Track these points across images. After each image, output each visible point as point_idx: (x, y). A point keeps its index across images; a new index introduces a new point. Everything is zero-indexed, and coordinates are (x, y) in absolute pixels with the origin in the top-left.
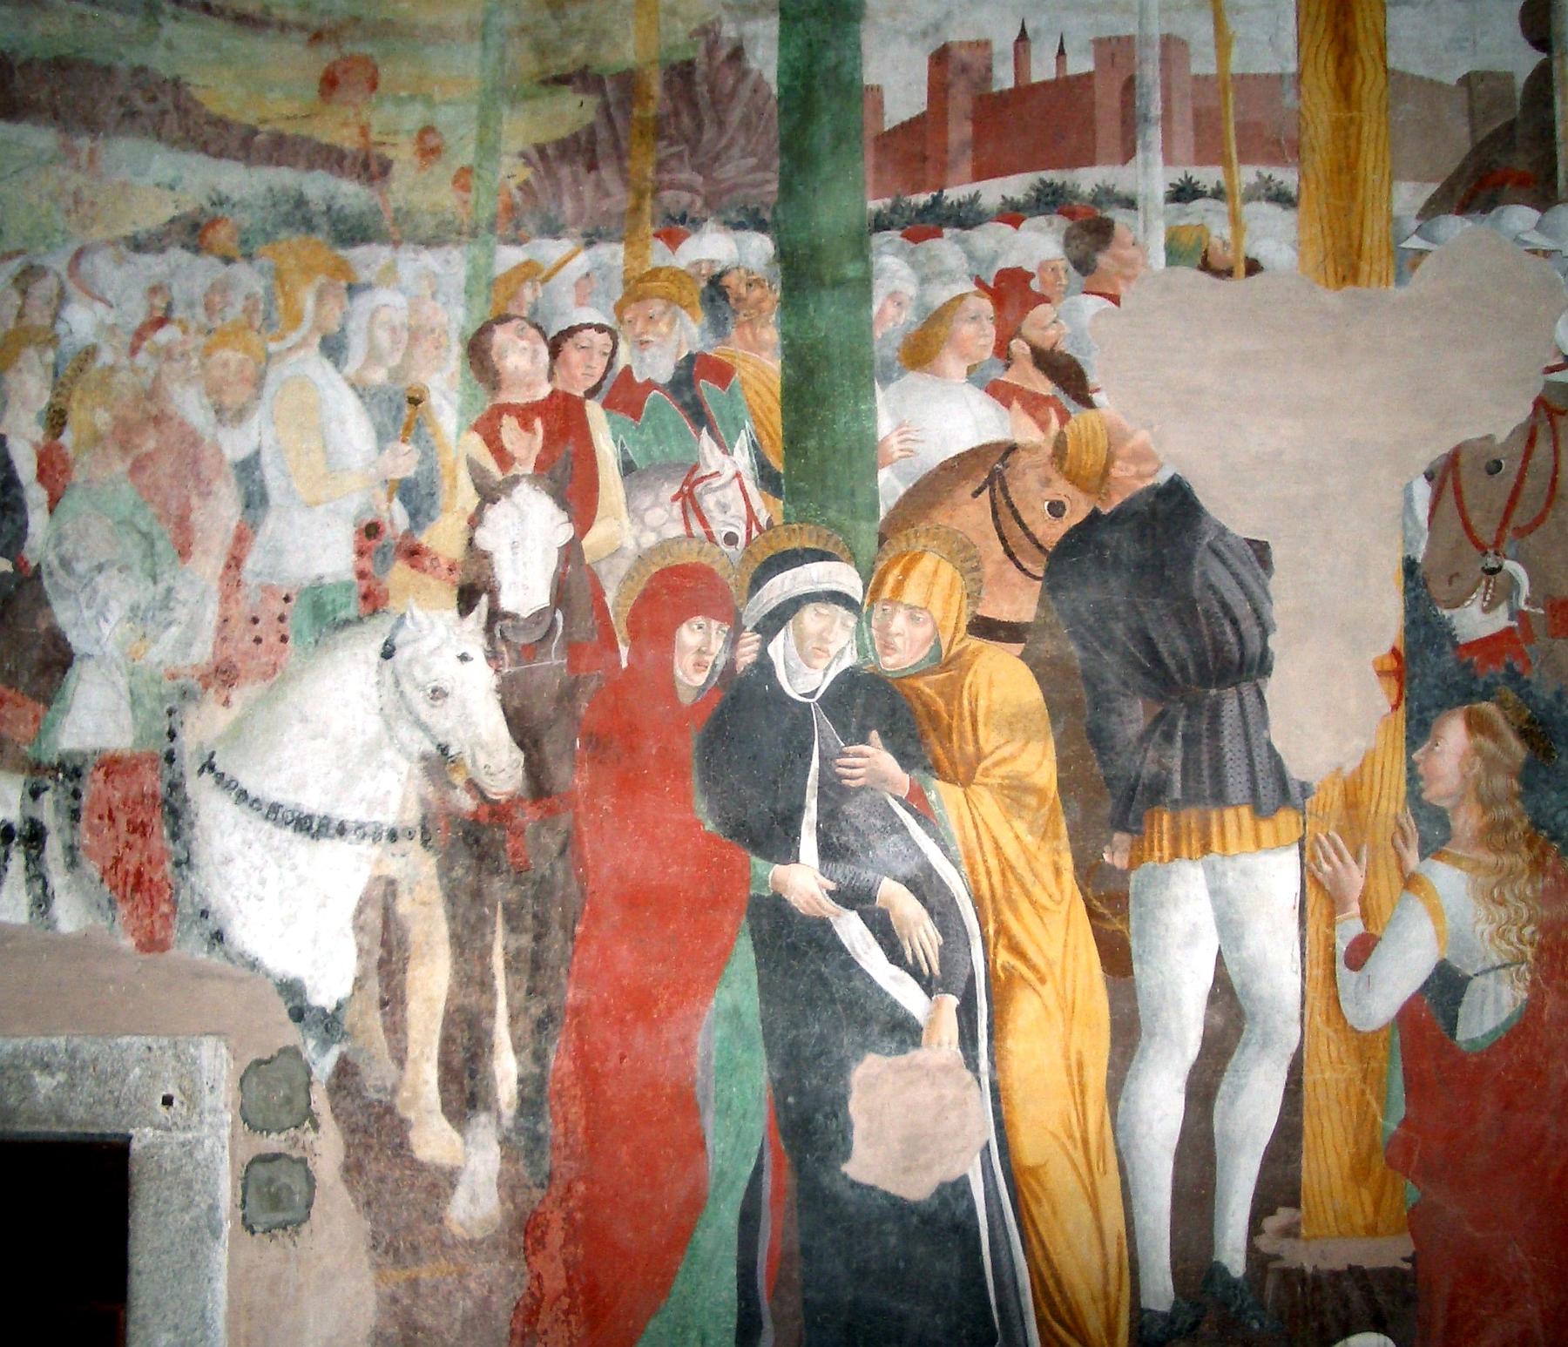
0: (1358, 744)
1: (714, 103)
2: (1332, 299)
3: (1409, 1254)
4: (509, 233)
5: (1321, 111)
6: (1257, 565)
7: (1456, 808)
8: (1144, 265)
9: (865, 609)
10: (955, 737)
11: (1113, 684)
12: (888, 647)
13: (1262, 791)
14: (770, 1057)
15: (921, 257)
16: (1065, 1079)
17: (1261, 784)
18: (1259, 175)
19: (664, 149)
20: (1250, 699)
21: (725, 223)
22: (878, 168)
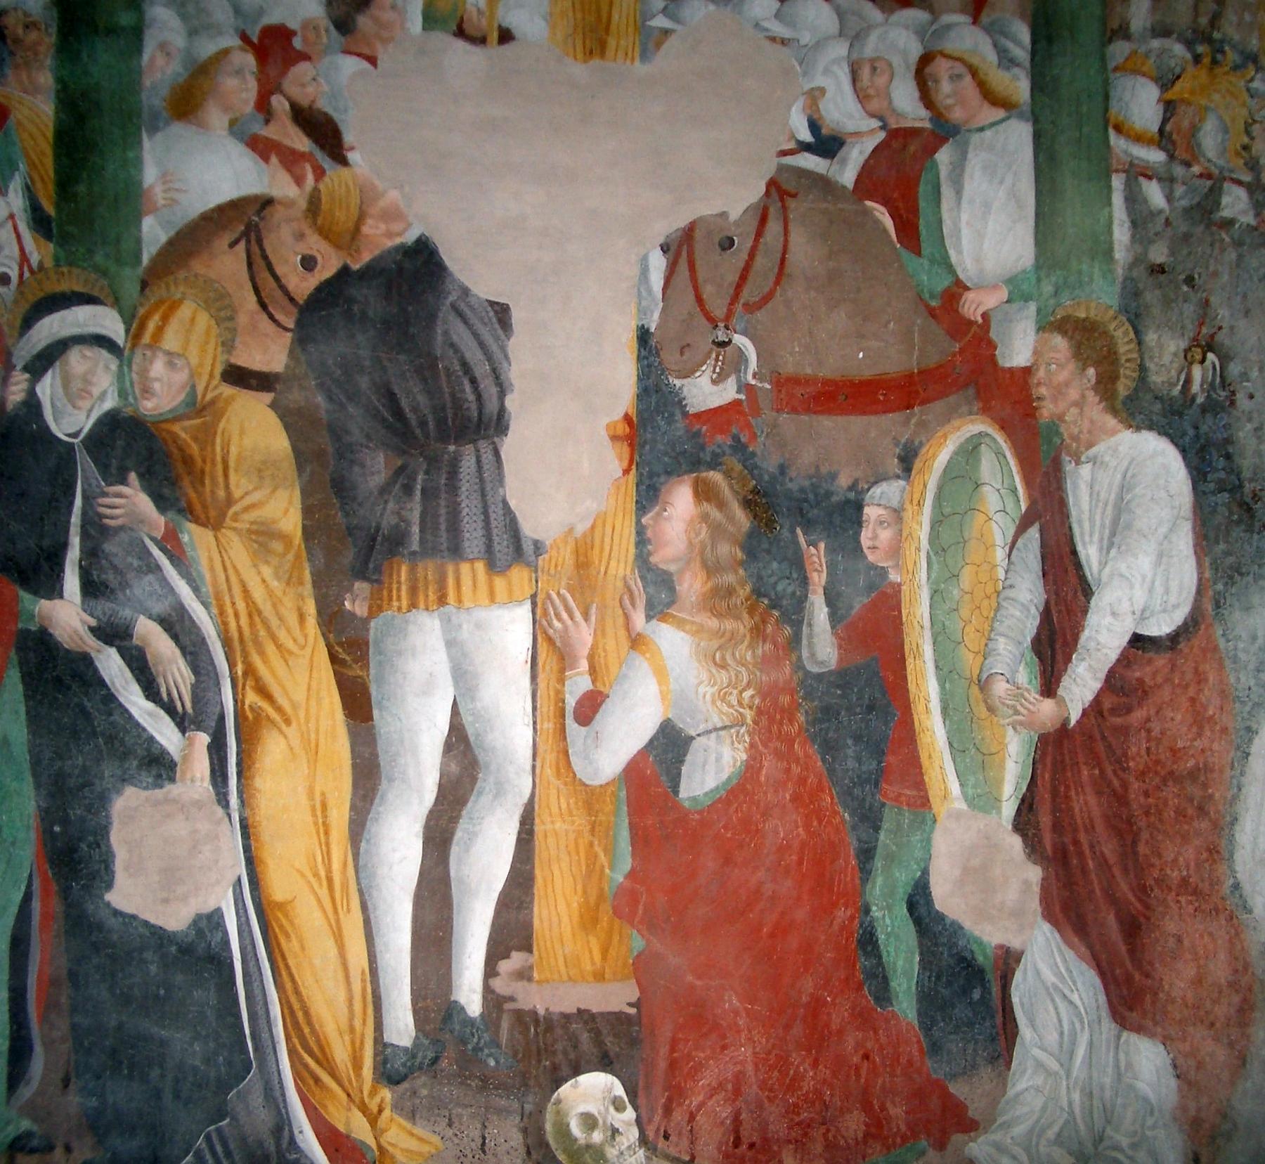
0: (590, 506)
2: (579, 70)
3: (634, 999)
6: (497, 326)
7: (681, 572)
9: (126, 353)
10: (207, 482)
11: (356, 435)
12: (147, 391)
13: (497, 548)
14: (38, 786)
16: (309, 819)
17: (496, 539)
20: (487, 457)
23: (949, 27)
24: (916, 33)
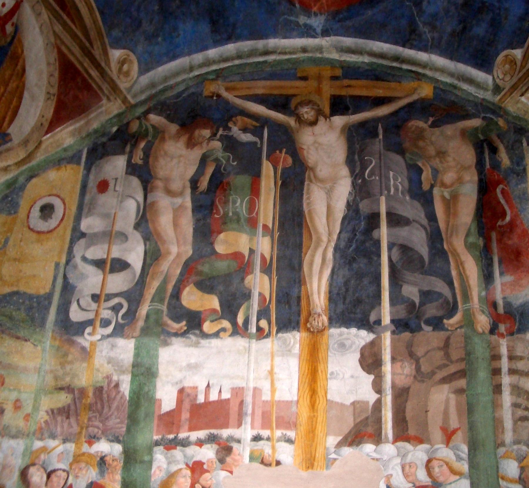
1: (108, 401)
2: (304, 474)
4: (40, 436)
5: (304, 412)
8: (242, 461)
15: (169, 455)
18: (282, 433)
19: (91, 414)
21: (108, 440)
22: (158, 426)
23: (437, 449)
24: (426, 452)
